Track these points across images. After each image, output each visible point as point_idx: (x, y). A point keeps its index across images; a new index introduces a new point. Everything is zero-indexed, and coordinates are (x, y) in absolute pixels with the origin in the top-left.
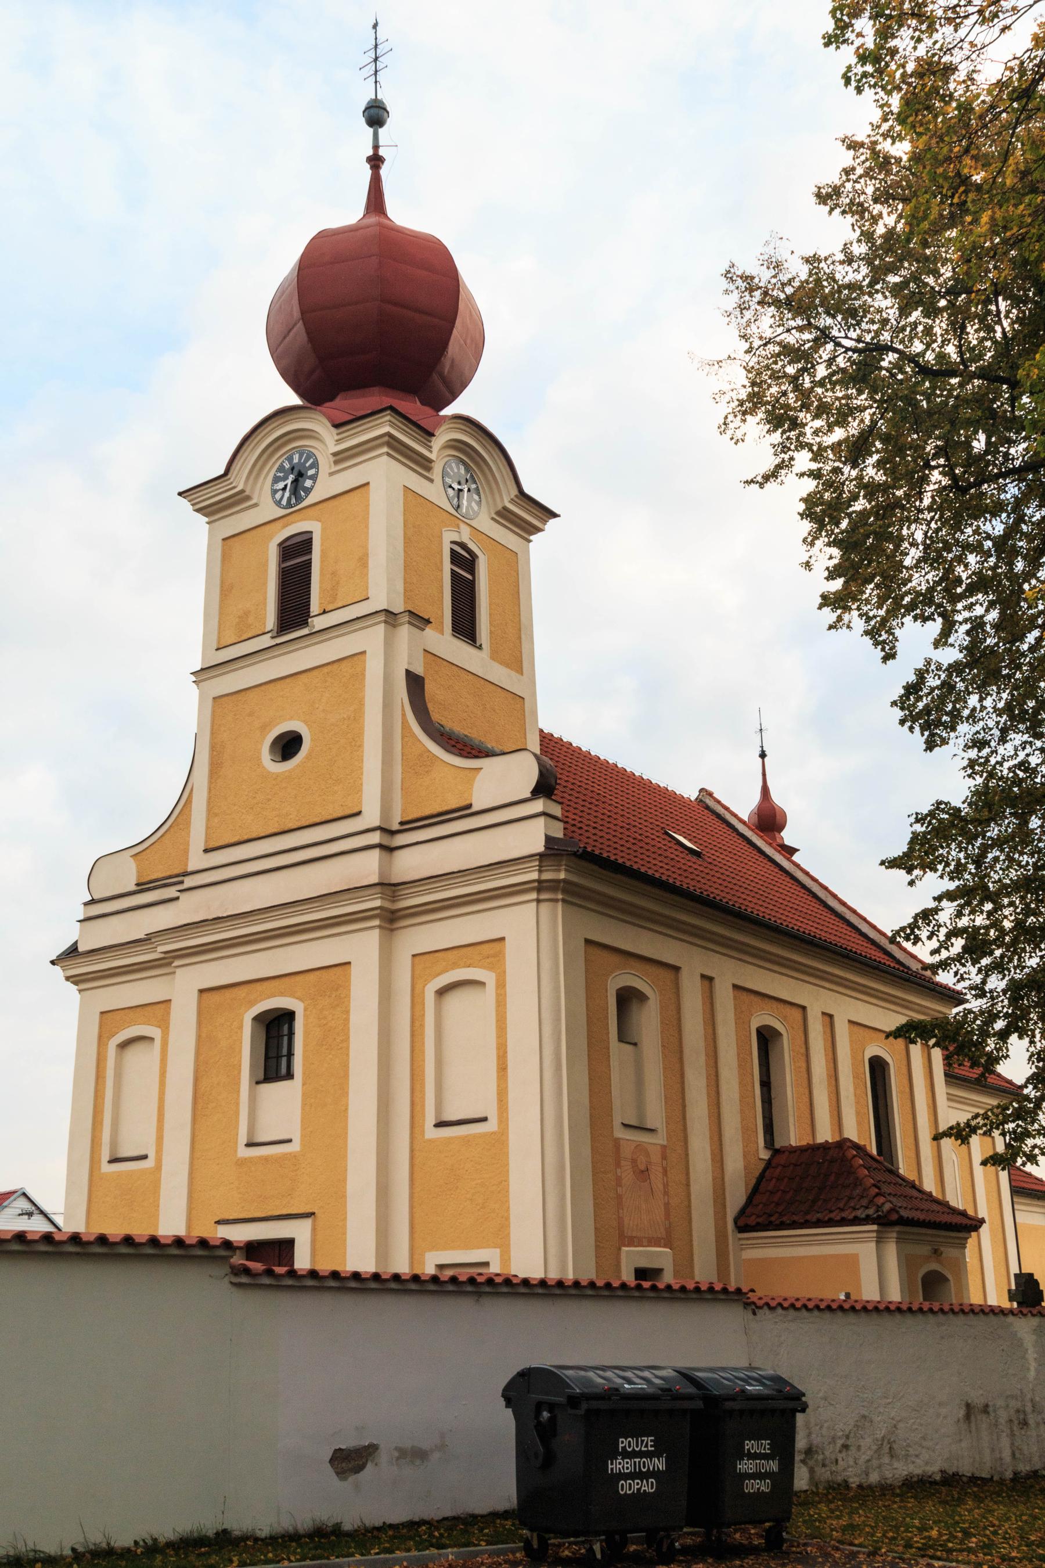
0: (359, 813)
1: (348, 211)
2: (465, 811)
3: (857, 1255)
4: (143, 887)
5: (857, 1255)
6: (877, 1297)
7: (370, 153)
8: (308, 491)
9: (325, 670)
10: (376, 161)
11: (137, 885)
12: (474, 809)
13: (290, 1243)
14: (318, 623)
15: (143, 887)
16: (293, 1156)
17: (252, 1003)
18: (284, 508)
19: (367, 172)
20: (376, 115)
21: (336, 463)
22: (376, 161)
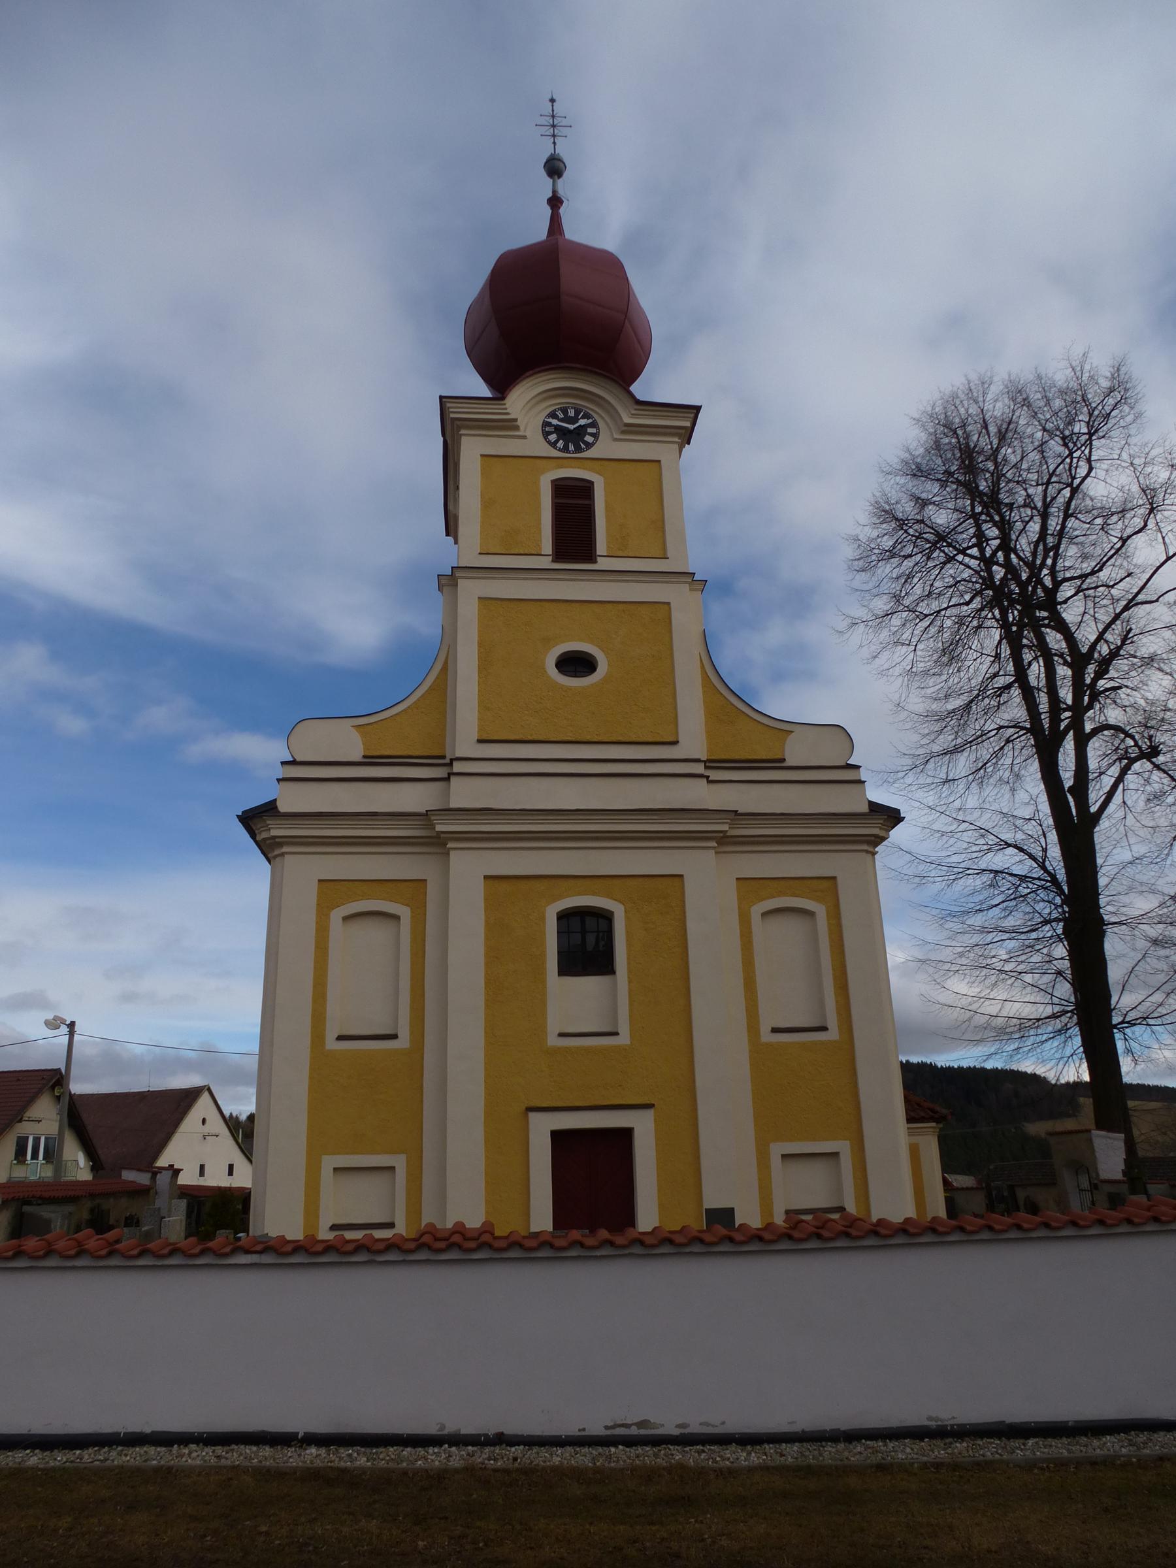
0: (676, 743)
1: (533, 230)
2: (778, 763)
3: (733, 1209)
4: (370, 760)
5: (733, 1209)
6: (911, 1212)
7: (550, 195)
8: (589, 446)
9: (621, 607)
10: (555, 202)
11: (364, 757)
12: (788, 763)
13: (626, 1135)
14: (603, 564)
15: (370, 760)
16: (618, 1049)
17: (555, 899)
18: (560, 450)
19: (548, 211)
20: (554, 168)
21: (623, 432)
22: (555, 202)
